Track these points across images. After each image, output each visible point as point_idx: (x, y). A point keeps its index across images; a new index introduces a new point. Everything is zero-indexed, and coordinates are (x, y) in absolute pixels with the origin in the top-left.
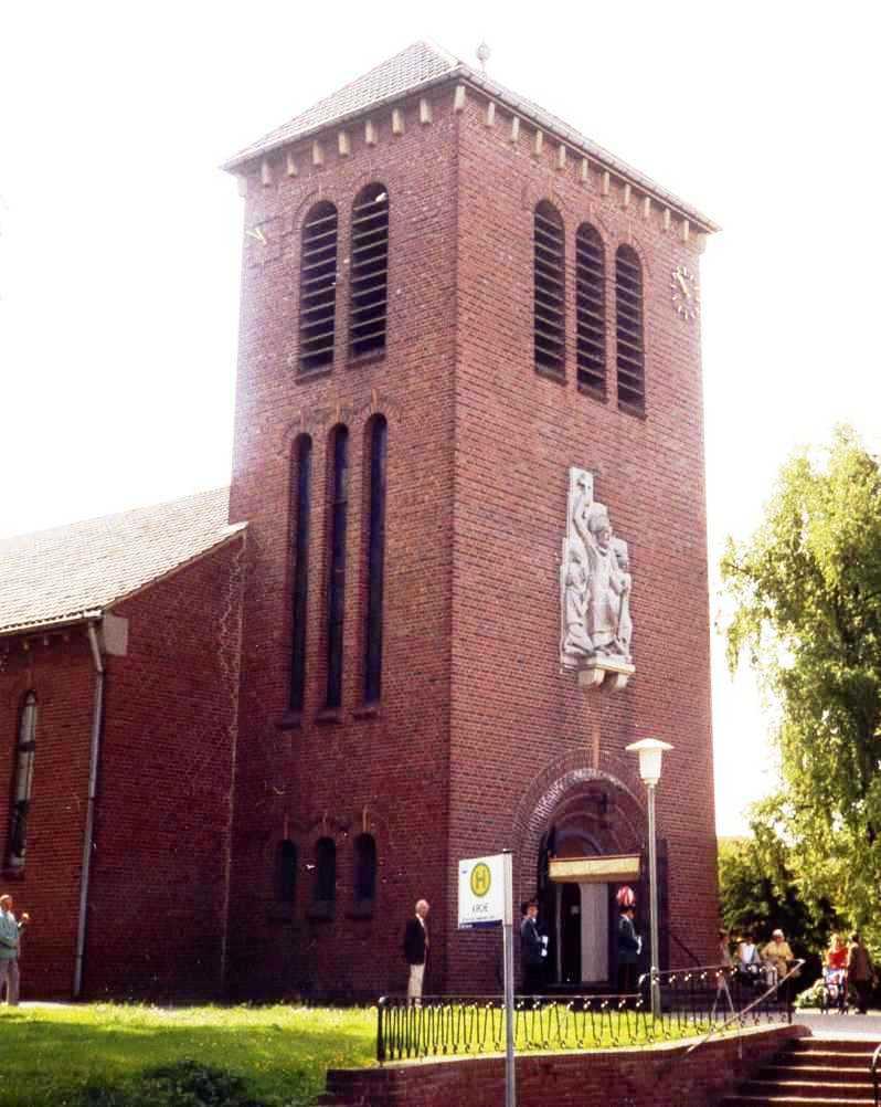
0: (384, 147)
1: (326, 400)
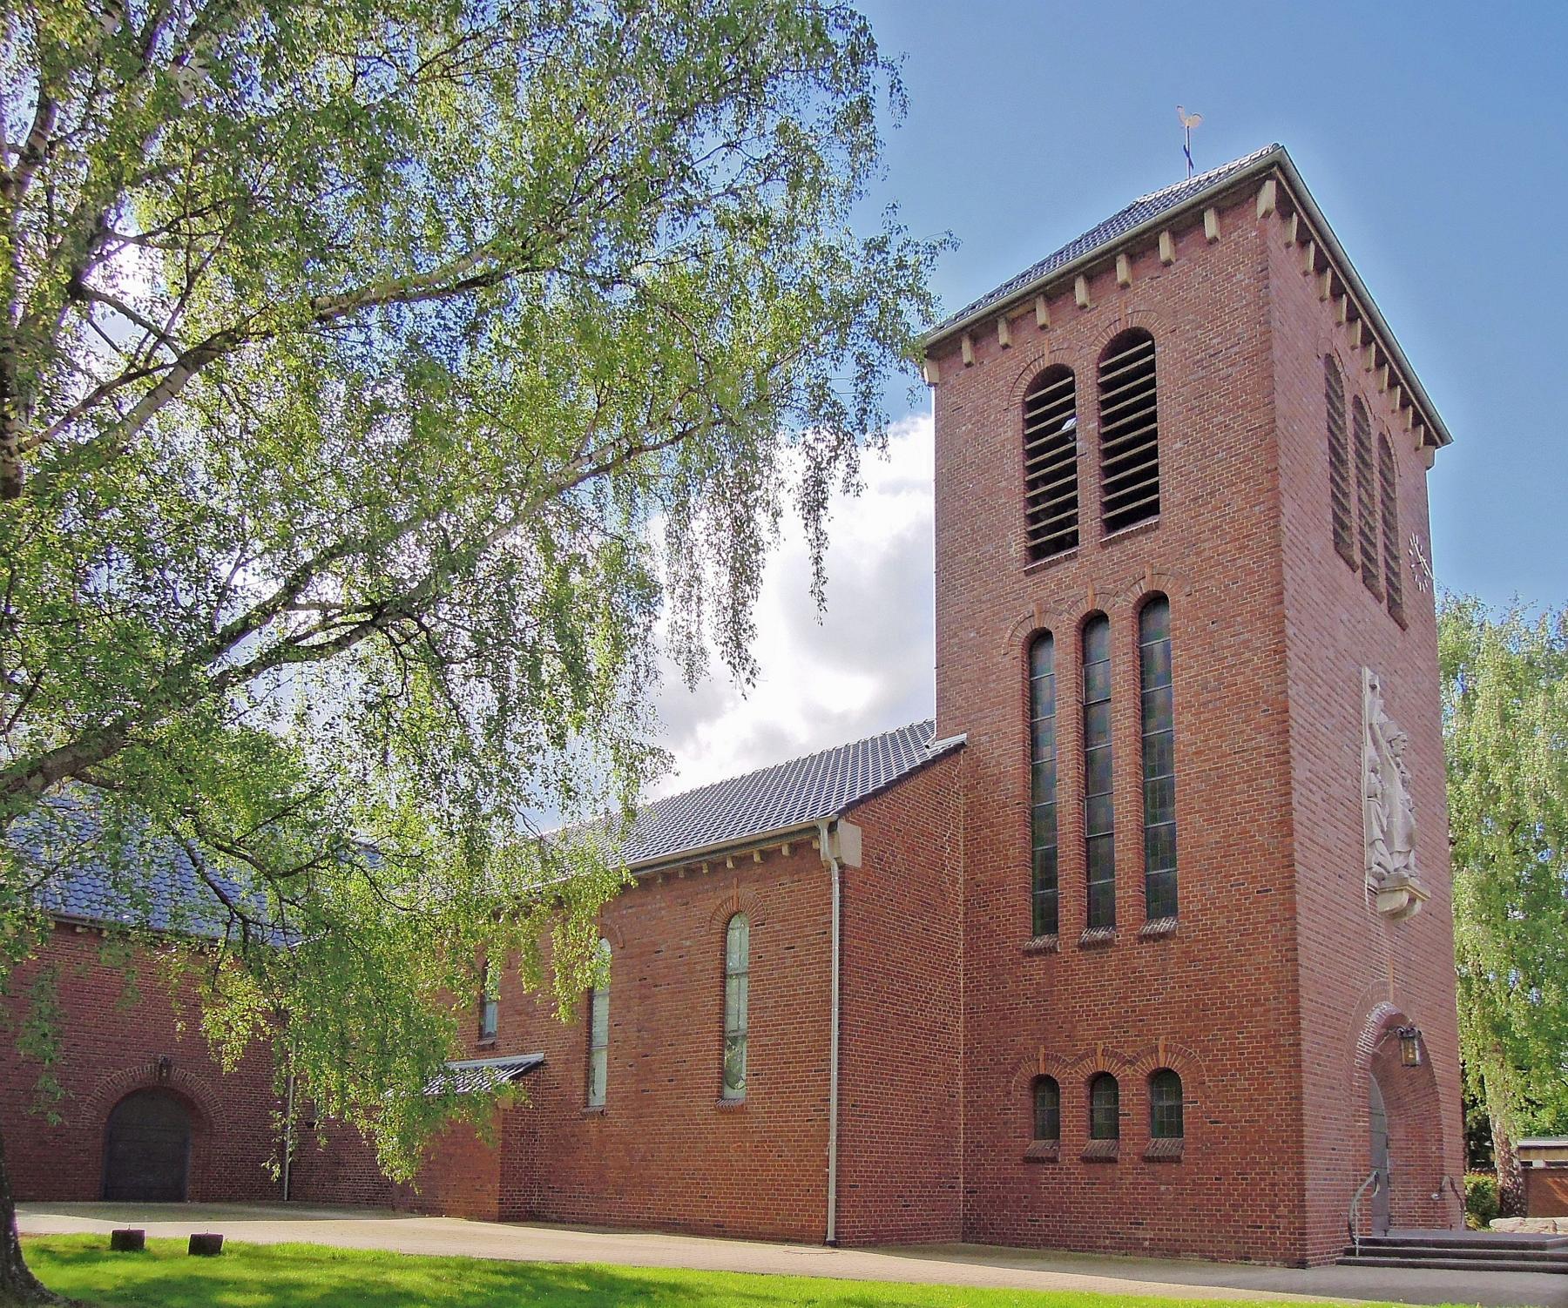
0: (1144, 284)
1: (1069, 587)
